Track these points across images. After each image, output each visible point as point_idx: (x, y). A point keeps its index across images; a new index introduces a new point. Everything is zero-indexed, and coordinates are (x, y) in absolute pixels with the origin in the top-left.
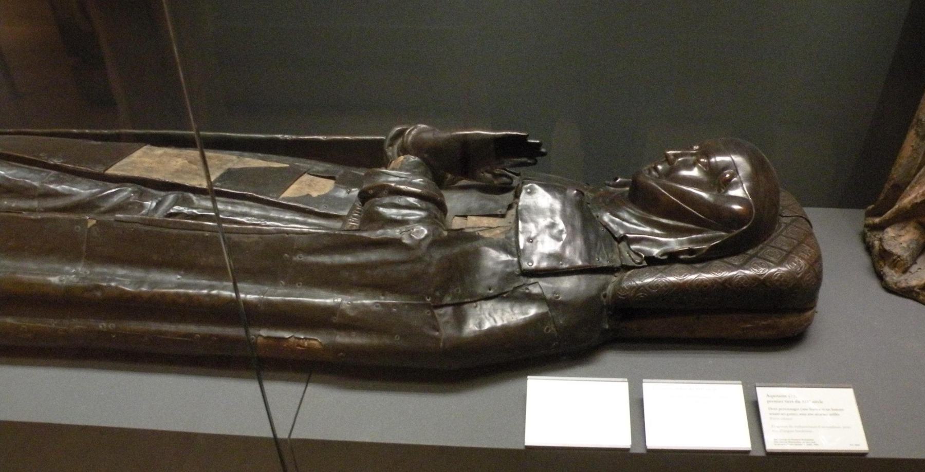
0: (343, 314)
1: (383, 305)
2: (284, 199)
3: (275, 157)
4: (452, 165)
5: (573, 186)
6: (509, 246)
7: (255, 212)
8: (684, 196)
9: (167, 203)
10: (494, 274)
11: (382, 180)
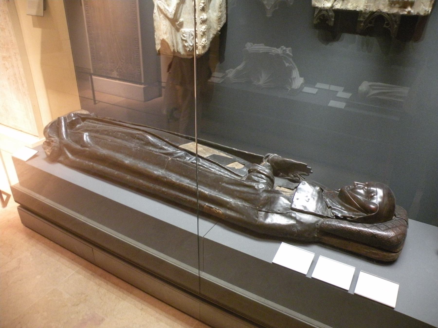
0: (231, 205)
1: (244, 205)
2: (228, 167)
3: (231, 155)
4: (280, 170)
5: (319, 186)
6: (291, 200)
7: (217, 169)
8: (355, 198)
9: (192, 159)
10: (282, 206)
11: (256, 168)
